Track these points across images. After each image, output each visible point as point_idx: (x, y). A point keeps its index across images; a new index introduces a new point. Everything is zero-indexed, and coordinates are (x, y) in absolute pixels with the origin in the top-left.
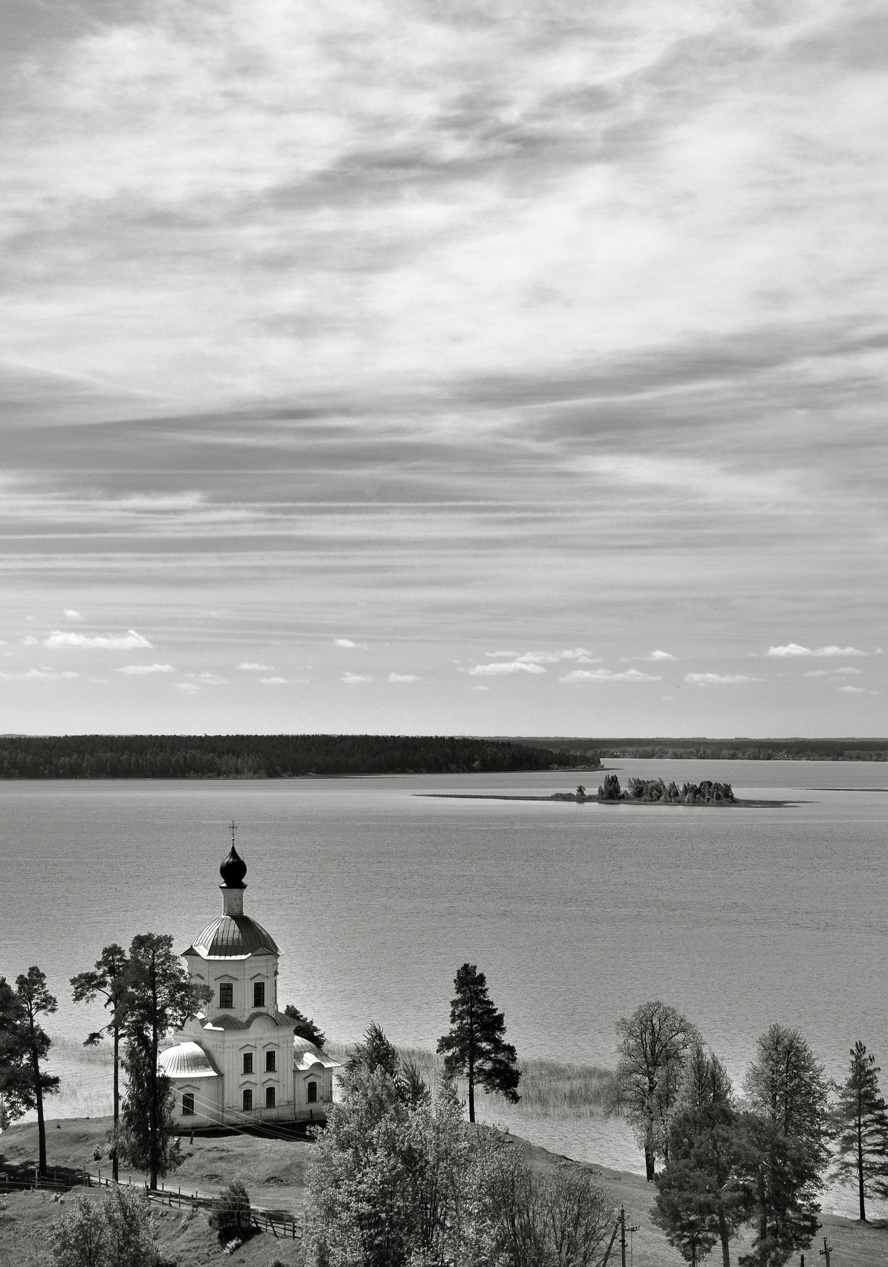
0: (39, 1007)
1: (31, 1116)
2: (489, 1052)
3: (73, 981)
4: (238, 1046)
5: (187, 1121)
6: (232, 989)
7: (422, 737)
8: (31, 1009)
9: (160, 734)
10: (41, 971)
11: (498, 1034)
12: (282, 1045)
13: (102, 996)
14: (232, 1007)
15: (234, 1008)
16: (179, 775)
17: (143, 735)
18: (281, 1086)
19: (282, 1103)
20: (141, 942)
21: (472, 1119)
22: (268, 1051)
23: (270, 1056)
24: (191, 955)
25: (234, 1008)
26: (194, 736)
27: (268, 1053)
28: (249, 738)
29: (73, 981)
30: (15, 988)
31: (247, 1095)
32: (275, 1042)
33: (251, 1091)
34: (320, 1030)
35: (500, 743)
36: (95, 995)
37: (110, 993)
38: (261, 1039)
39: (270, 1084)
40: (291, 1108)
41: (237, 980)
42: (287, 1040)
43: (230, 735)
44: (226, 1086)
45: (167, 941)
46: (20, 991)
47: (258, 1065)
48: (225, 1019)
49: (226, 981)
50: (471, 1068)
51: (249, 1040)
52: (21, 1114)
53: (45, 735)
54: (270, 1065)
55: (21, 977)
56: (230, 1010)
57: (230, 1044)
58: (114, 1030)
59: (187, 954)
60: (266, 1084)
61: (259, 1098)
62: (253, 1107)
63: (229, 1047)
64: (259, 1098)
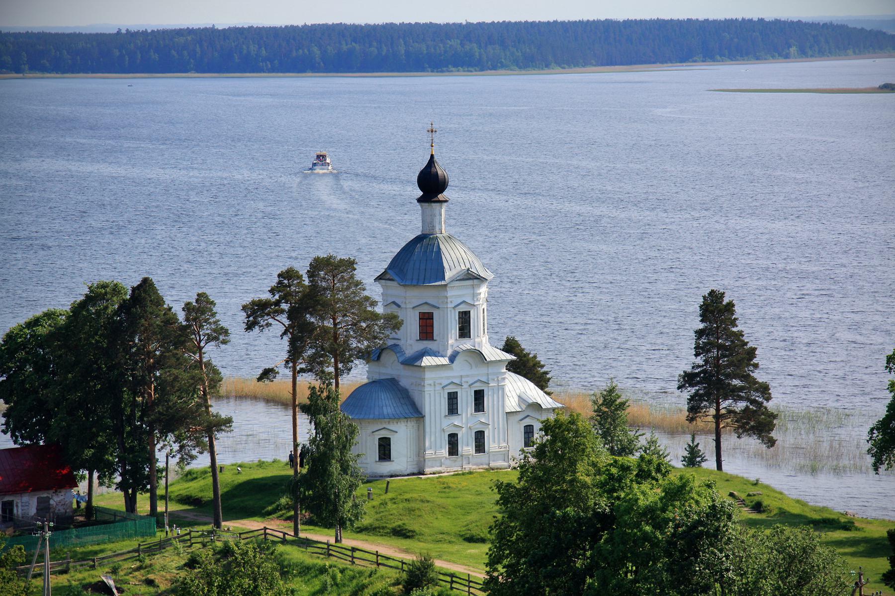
0: (210, 339)
1: (202, 462)
2: (741, 389)
3: (244, 308)
4: (441, 384)
6: (433, 319)
8: (200, 341)
10: (211, 298)
13: (278, 325)
16: (793, 50)
21: (719, 467)
23: (479, 396)
24: (384, 279)
29: (244, 308)
30: (181, 317)
33: (457, 434)
36: (271, 324)
37: (287, 323)
38: (468, 376)
41: (438, 308)
44: (428, 429)
45: (350, 264)
46: (187, 320)
48: (425, 352)
49: (426, 309)
50: (718, 410)
51: (454, 377)
52: (193, 458)
55: (188, 304)
57: (429, 382)
59: (380, 279)
63: (431, 385)
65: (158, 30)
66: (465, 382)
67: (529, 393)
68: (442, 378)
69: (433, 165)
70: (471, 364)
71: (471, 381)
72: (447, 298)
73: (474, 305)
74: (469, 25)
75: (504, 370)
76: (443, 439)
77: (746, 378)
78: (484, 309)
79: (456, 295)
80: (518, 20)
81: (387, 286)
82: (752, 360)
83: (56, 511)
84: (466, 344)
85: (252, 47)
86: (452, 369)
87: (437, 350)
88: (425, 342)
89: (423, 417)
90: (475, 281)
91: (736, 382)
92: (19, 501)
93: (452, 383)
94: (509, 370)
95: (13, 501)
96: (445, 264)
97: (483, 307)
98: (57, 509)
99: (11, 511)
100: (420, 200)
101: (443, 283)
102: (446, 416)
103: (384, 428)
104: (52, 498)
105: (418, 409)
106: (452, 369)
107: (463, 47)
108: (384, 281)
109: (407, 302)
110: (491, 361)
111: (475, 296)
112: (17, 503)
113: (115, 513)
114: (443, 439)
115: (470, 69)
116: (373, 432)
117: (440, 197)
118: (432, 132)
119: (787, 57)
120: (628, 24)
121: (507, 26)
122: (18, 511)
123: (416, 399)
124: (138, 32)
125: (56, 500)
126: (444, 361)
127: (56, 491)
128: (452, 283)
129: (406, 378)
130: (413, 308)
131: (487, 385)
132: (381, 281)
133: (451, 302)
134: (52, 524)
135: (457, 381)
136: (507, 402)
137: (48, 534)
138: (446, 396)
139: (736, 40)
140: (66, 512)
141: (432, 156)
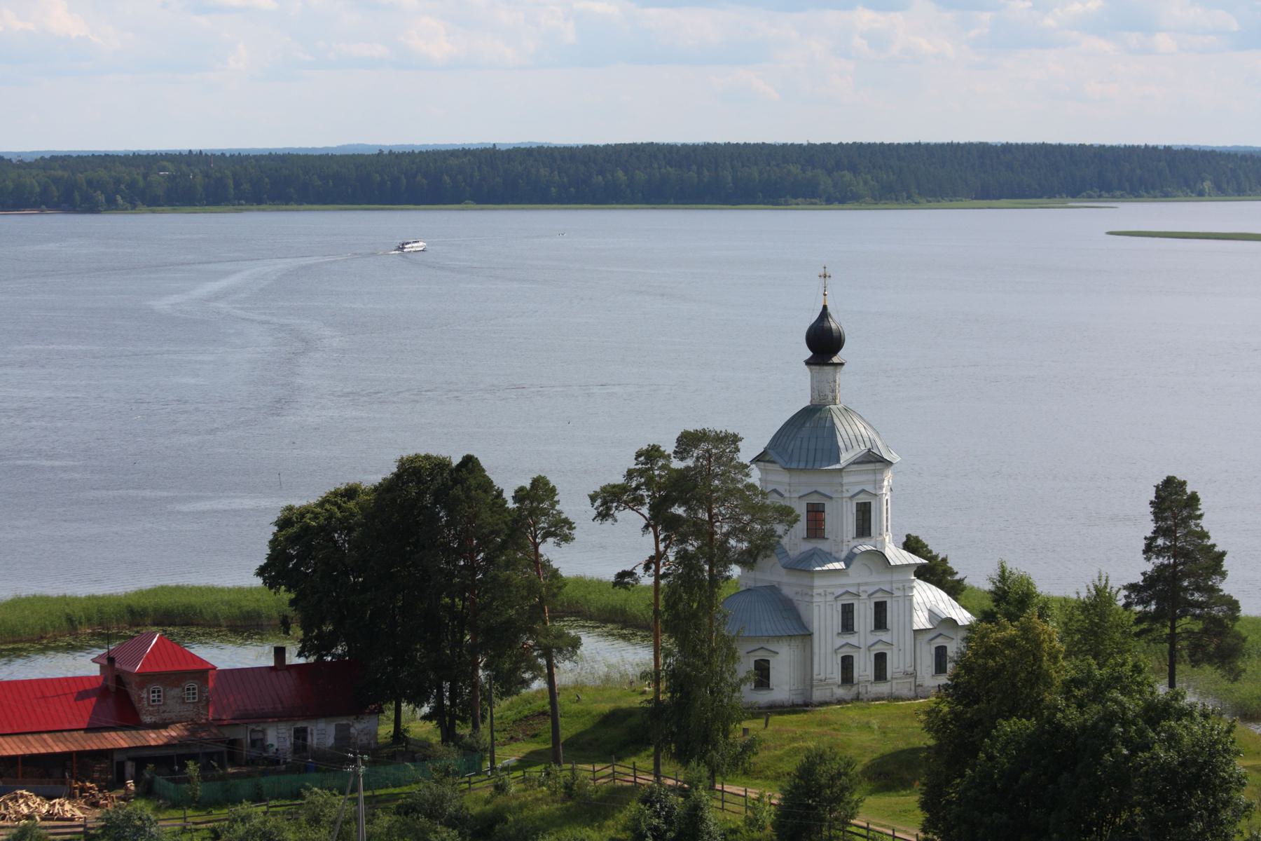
4: (833, 594)
5: (763, 698)
7: (1125, 146)
9: (741, 141)
11: (1215, 581)
12: (897, 593)
14: (824, 538)
15: (827, 539)
16: (1207, 185)
17: (718, 142)
18: (895, 651)
19: (897, 675)
20: (688, 441)
22: (878, 600)
23: (880, 608)
24: (764, 461)
25: (827, 539)
26: (792, 144)
27: (877, 604)
28: (870, 146)
31: (847, 663)
32: (887, 588)
34: (957, 573)
35: (1239, 156)
38: (866, 584)
39: (879, 648)
40: (910, 682)
41: (831, 498)
42: (904, 586)
43: (844, 142)
44: (816, 650)
45: (735, 439)
47: (862, 620)
48: (814, 554)
49: (815, 499)
53: (1075, 143)
54: (880, 622)
56: (820, 541)
57: (820, 591)
58: (653, 567)
59: (758, 461)
60: (873, 648)
61: (864, 668)
62: (855, 681)
64: (864, 668)
65: (427, 151)
66: (863, 591)
67: (942, 606)
68: (835, 586)
69: (826, 319)
70: (869, 568)
71: (871, 589)
72: (842, 485)
73: (876, 495)
74: (811, 147)
75: (913, 578)
76: (835, 662)
77: (1213, 590)
78: (887, 500)
79: (854, 482)
80: (872, 141)
81: (766, 470)
82: (1160, 569)
83: (359, 742)
84: (866, 546)
85: (542, 171)
86: (848, 575)
87: (829, 551)
88: (813, 541)
89: (811, 635)
90: (877, 464)
91: (1197, 596)
92: (314, 728)
93: (847, 592)
94: (918, 578)
95: (307, 727)
96: (841, 444)
97: (887, 498)
98: (359, 739)
99: (305, 739)
100: (808, 363)
101: (838, 466)
102: (839, 634)
103: (762, 648)
104: (352, 726)
105: (803, 624)
106: (848, 575)
107: (804, 172)
108: (762, 464)
109: (792, 490)
110: (896, 566)
111: (878, 484)
112: (312, 730)
113: (1046, 604)
114: (835, 662)
115: (813, 200)
116: (748, 653)
117: (835, 360)
118: (825, 277)
119: (1201, 194)
120: (1007, 148)
121: (859, 148)
122: (313, 740)
123: (802, 609)
124: (404, 153)
125: (358, 728)
126: (839, 565)
127: (357, 717)
128: (849, 467)
129: (789, 585)
130: (800, 497)
131: (890, 595)
132: (759, 463)
133: (847, 491)
134: (366, 757)
135: (853, 590)
136: (915, 618)
137: (362, 769)
138: (840, 609)
139: (1138, 171)
140: (369, 744)
141: (825, 307)
